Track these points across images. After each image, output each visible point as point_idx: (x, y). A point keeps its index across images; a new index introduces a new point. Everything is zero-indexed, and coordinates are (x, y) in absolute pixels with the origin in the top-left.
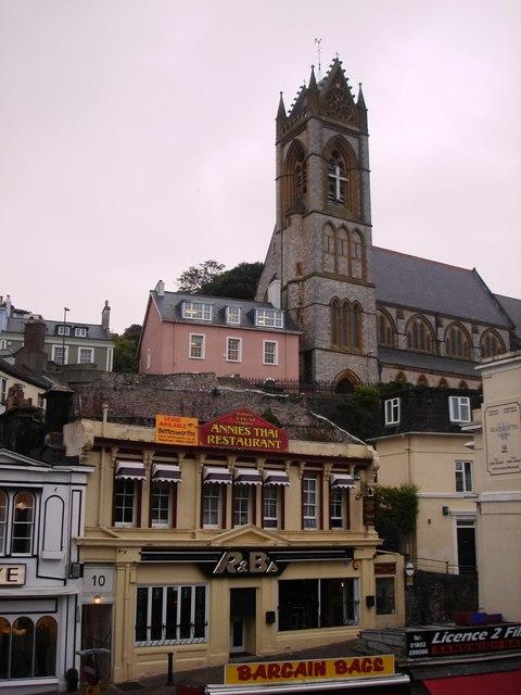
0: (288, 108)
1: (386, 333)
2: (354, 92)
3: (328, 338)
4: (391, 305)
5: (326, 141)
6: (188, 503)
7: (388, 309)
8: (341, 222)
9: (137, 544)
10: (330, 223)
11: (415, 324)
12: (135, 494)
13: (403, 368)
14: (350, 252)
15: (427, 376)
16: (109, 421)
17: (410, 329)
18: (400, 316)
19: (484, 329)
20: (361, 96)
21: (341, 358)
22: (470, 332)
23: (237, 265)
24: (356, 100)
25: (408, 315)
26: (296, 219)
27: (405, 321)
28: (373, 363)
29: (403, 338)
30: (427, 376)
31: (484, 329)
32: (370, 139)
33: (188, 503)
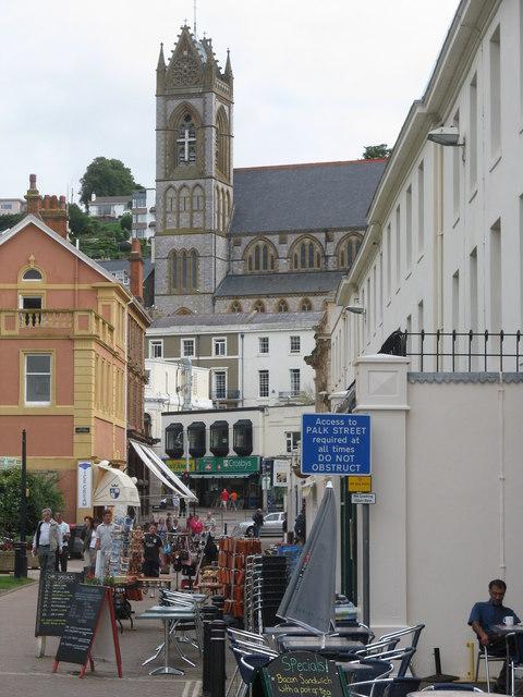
0: (168, 55)
1: (269, 259)
2: (222, 64)
3: (165, 285)
5: (170, 111)
7: (270, 238)
8: (182, 182)
9: (476, 663)
11: (303, 245)
12: (35, 538)
13: (237, 297)
14: (192, 206)
15: (264, 300)
16: (71, 401)
21: (176, 299)
22: (243, 246)
24: (222, 72)
25: (338, 236)
29: (285, 261)
30: (264, 300)
32: (235, 108)
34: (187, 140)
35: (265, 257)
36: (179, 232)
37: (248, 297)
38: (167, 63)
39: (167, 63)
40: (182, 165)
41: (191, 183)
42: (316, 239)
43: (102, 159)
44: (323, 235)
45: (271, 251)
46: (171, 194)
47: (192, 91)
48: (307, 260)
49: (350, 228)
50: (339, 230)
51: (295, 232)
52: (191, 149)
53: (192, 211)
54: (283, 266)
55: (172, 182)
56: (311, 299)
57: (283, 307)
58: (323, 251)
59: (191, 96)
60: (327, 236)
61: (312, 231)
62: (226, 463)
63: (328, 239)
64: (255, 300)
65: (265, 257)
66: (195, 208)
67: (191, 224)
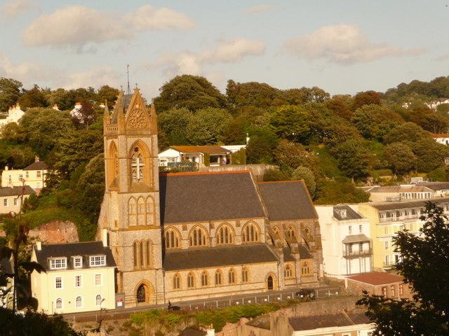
8: (139, 194)
21: (139, 274)
22: (234, 227)
28: (160, 272)
36: (139, 228)
41: (145, 195)
42: (204, 227)
43: (107, 87)
48: (198, 241)
55: (133, 194)
58: (209, 234)
60: (210, 225)
67: (138, 224)
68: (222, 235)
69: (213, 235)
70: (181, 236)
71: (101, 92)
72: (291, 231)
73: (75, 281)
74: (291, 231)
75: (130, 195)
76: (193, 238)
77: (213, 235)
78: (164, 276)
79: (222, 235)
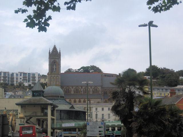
4: (71, 86)
5: (52, 61)
6: (21, 77)
10: (52, 76)
17: (75, 90)
18: (72, 88)
19: (84, 87)
20: (60, 52)
22: (90, 88)
23: (180, 70)
24: (59, 52)
25: (74, 87)
26: (154, 23)
27: (83, 89)
31: (84, 87)
33: (21, 77)
34: (55, 67)
35: (97, 91)
37: (68, 98)
38: (51, 52)
39: (51, 52)
40: (53, 72)
41: (56, 76)
42: (79, 88)
44: (81, 87)
45: (70, 90)
46: (52, 78)
47: (56, 58)
49: (95, 86)
50: (84, 86)
51: (75, 86)
52: (55, 69)
53: (56, 81)
54: (72, 92)
56: (71, 99)
57: (80, 101)
59: (56, 59)
61: (78, 86)
62: (115, 132)
63: (82, 88)
64: (79, 99)
65: (97, 91)
66: (57, 81)
67: (56, 84)
68: (95, 91)
69: (82, 90)
70: (90, 90)
71: (29, 6)
72: (106, 91)
73: (6, 108)
74: (106, 91)
75: (51, 76)
76: (94, 91)
77: (82, 90)
78: (60, 50)
79: (95, 91)
